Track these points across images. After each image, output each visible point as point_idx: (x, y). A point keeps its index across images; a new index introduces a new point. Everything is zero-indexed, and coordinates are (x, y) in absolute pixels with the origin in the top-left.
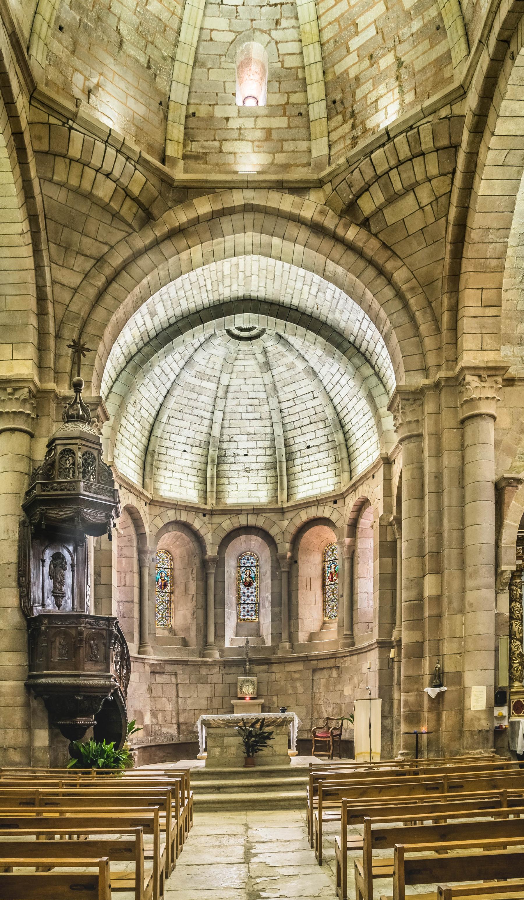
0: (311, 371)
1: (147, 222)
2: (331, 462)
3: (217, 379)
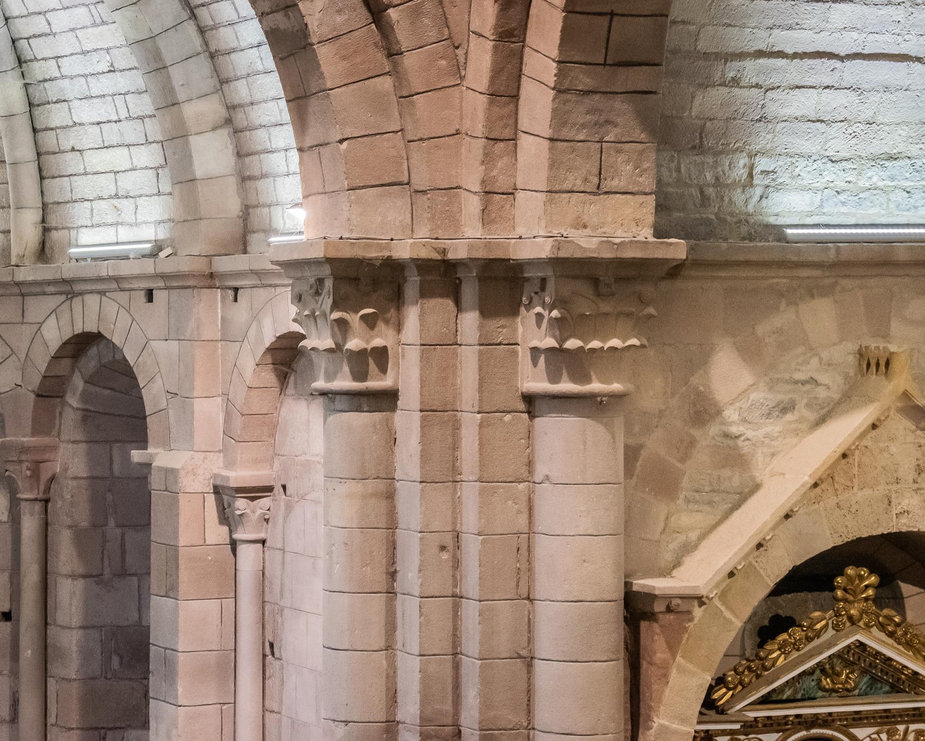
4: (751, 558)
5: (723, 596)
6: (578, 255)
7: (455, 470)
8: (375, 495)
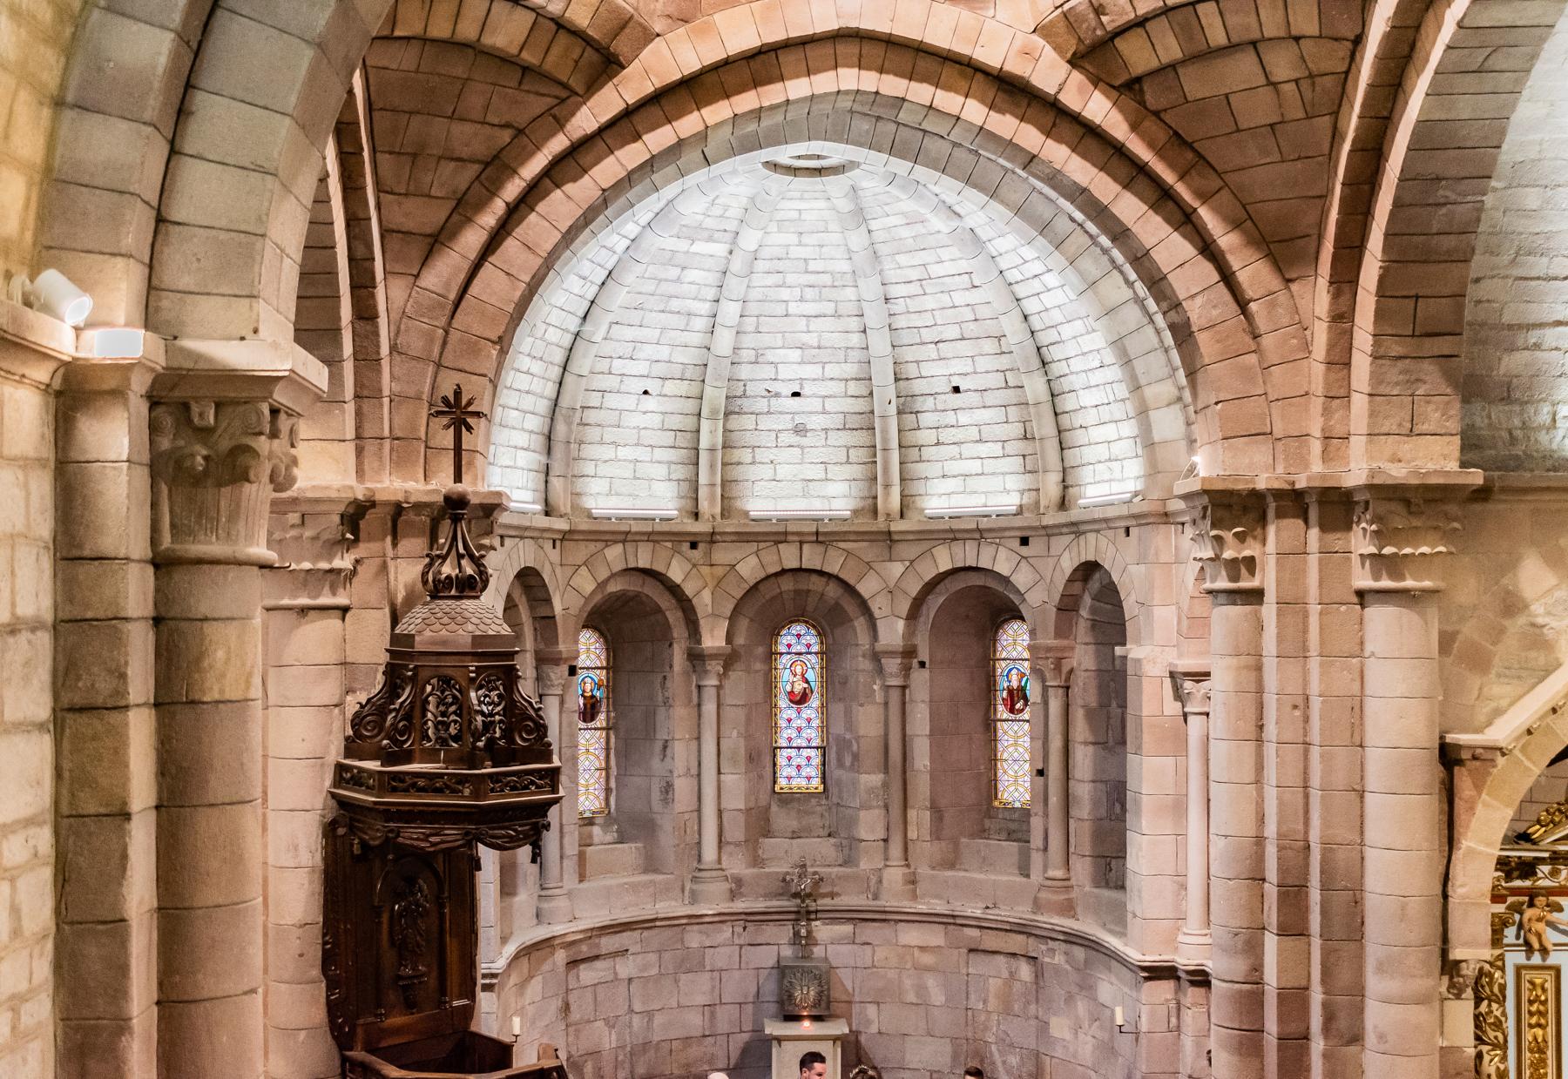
0: (968, 236)
1: (604, 71)
2: (1013, 436)
3: (728, 237)
4: (1548, 720)
5: (1524, 749)
6: (1389, 482)
7: (1305, 648)
8: (1247, 667)
